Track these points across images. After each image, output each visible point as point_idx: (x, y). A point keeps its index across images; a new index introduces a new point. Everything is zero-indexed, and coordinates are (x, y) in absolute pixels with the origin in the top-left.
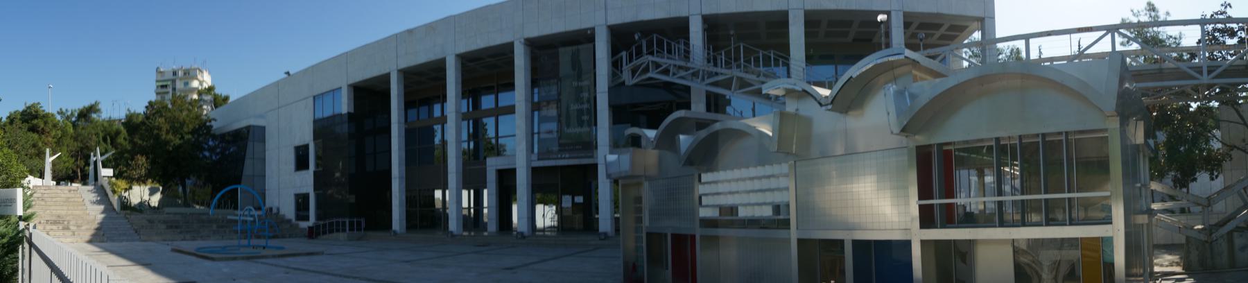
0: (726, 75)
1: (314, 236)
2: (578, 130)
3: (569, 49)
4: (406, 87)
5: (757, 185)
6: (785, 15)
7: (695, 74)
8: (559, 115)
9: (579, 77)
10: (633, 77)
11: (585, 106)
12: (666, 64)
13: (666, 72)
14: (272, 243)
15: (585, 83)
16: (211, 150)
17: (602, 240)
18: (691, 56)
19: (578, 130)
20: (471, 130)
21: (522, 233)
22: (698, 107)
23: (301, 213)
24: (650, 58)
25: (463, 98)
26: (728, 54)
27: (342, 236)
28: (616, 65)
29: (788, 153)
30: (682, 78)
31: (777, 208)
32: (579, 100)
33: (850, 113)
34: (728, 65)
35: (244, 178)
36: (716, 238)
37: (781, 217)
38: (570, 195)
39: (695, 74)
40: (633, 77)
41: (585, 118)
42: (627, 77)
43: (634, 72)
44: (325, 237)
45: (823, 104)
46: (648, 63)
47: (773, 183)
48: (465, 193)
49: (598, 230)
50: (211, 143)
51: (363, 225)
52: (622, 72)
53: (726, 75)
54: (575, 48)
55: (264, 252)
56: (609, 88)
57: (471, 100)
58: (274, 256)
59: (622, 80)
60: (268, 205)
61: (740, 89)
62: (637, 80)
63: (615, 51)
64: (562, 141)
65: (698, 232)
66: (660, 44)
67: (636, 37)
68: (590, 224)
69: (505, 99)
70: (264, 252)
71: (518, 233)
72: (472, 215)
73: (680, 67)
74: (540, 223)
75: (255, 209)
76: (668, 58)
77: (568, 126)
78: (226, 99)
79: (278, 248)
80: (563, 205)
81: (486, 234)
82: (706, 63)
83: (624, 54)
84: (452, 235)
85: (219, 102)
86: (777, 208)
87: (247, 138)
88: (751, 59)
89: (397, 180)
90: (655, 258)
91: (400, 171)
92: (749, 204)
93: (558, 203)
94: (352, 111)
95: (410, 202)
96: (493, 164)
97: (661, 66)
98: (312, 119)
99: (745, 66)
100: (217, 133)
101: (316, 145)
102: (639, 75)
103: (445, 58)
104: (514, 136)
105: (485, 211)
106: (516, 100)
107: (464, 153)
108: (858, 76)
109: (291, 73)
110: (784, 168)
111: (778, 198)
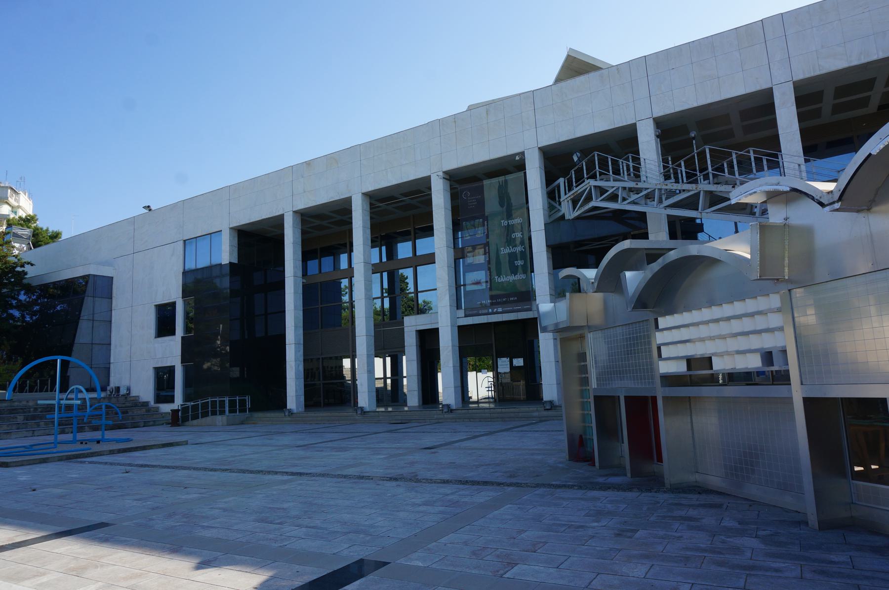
0: (689, 191)
1: (180, 422)
2: (512, 278)
3: (495, 181)
4: (304, 233)
5: (747, 324)
6: (768, 94)
7: (649, 196)
8: (489, 262)
9: (509, 216)
10: (574, 209)
11: (519, 249)
12: (613, 187)
13: (614, 198)
14: (109, 435)
15: (517, 221)
16: (20, 306)
17: (548, 410)
18: (642, 173)
19: (512, 278)
20: (386, 286)
21: (448, 406)
22: (658, 235)
23: (163, 393)
24: (593, 183)
25: (372, 247)
26: (690, 164)
27: (219, 419)
28: (552, 196)
29: (778, 280)
30: (634, 203)
31: (768, 357)
32: (510, 242)
33: (875, 209)
34: (691, 178)
35: (75, 348)
36: (688, 400)
37: (775, 368)
38: (507, 358)
39: (649, 196)
40: (574, 209)
41: (520, 263)
42: (567, 210)
43: (575, 202)
44: (195, 422)
45: (826, 203)
46: (591, 189)
47: (760, 323)
48: (378, 362)
49: (542, 399)
50: (22, 297)
51: (248, 405)
52: (560, 204)
53: (689, 191)
54: (501, 179)
55: (96, 448)
56: (546, 225)
57: (384, 248)
58: (112, 452)
59: (561, 214)
60: (114, 382)
61: (710, 206)
62: (579, 212)
63: (550, 178)
64: (494, 293)
65: (660, 392)
66: (603, 164)
67: (575, 159)
68: (534, 392)
69: (423, 246)
70: (96, 448)
71: (443, 406)
72: (389, 388)
73: (631, 190)
74: (473, 394)
75: (88, 390)
76: (614, 180)
77: (499, 275)
78: (55, 236)
79: (118, 441)
80: (499, 371)
81: (406, 409)
82: (662, 179)
83: (561, 181)
84: (363, 411)
85: (38, 239)
86: (768, 357)
87: (84, 292)
88: (723, 165)
89: (293, 346)
90: (607, 429)
91: (296, 335)
92: (728, 353)
93: (494, 368)
94: (235, 261)
95: (309, 375)
96: (412, 324)
97: (607, 191)
98: (181, 270)
99: (714, 176)
100: (35, 283)
101: (186, 304)
102: (581, 206)
103: (351, 197)
104: (436, 289)
105: (405, 381)
106: (436, 247)
107: (376, 313)
108: (881, 151)
109: (153, 208)
110: (775, 300)
111: (769, 342)
